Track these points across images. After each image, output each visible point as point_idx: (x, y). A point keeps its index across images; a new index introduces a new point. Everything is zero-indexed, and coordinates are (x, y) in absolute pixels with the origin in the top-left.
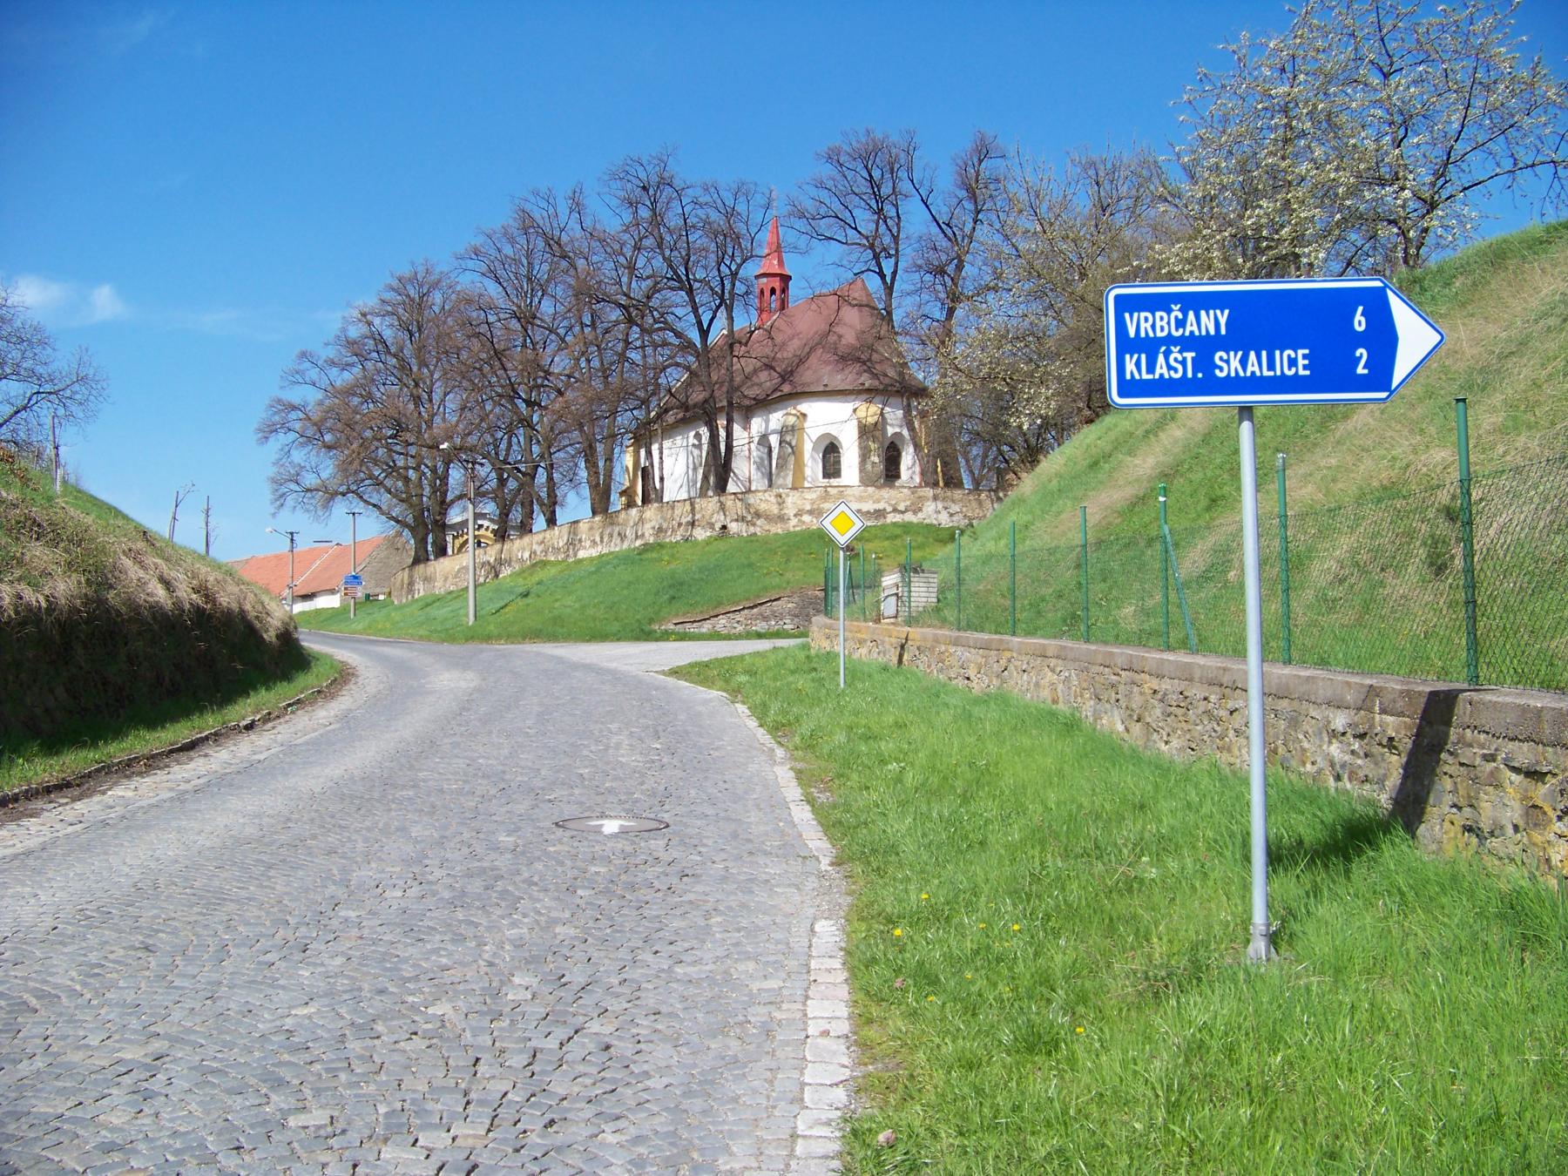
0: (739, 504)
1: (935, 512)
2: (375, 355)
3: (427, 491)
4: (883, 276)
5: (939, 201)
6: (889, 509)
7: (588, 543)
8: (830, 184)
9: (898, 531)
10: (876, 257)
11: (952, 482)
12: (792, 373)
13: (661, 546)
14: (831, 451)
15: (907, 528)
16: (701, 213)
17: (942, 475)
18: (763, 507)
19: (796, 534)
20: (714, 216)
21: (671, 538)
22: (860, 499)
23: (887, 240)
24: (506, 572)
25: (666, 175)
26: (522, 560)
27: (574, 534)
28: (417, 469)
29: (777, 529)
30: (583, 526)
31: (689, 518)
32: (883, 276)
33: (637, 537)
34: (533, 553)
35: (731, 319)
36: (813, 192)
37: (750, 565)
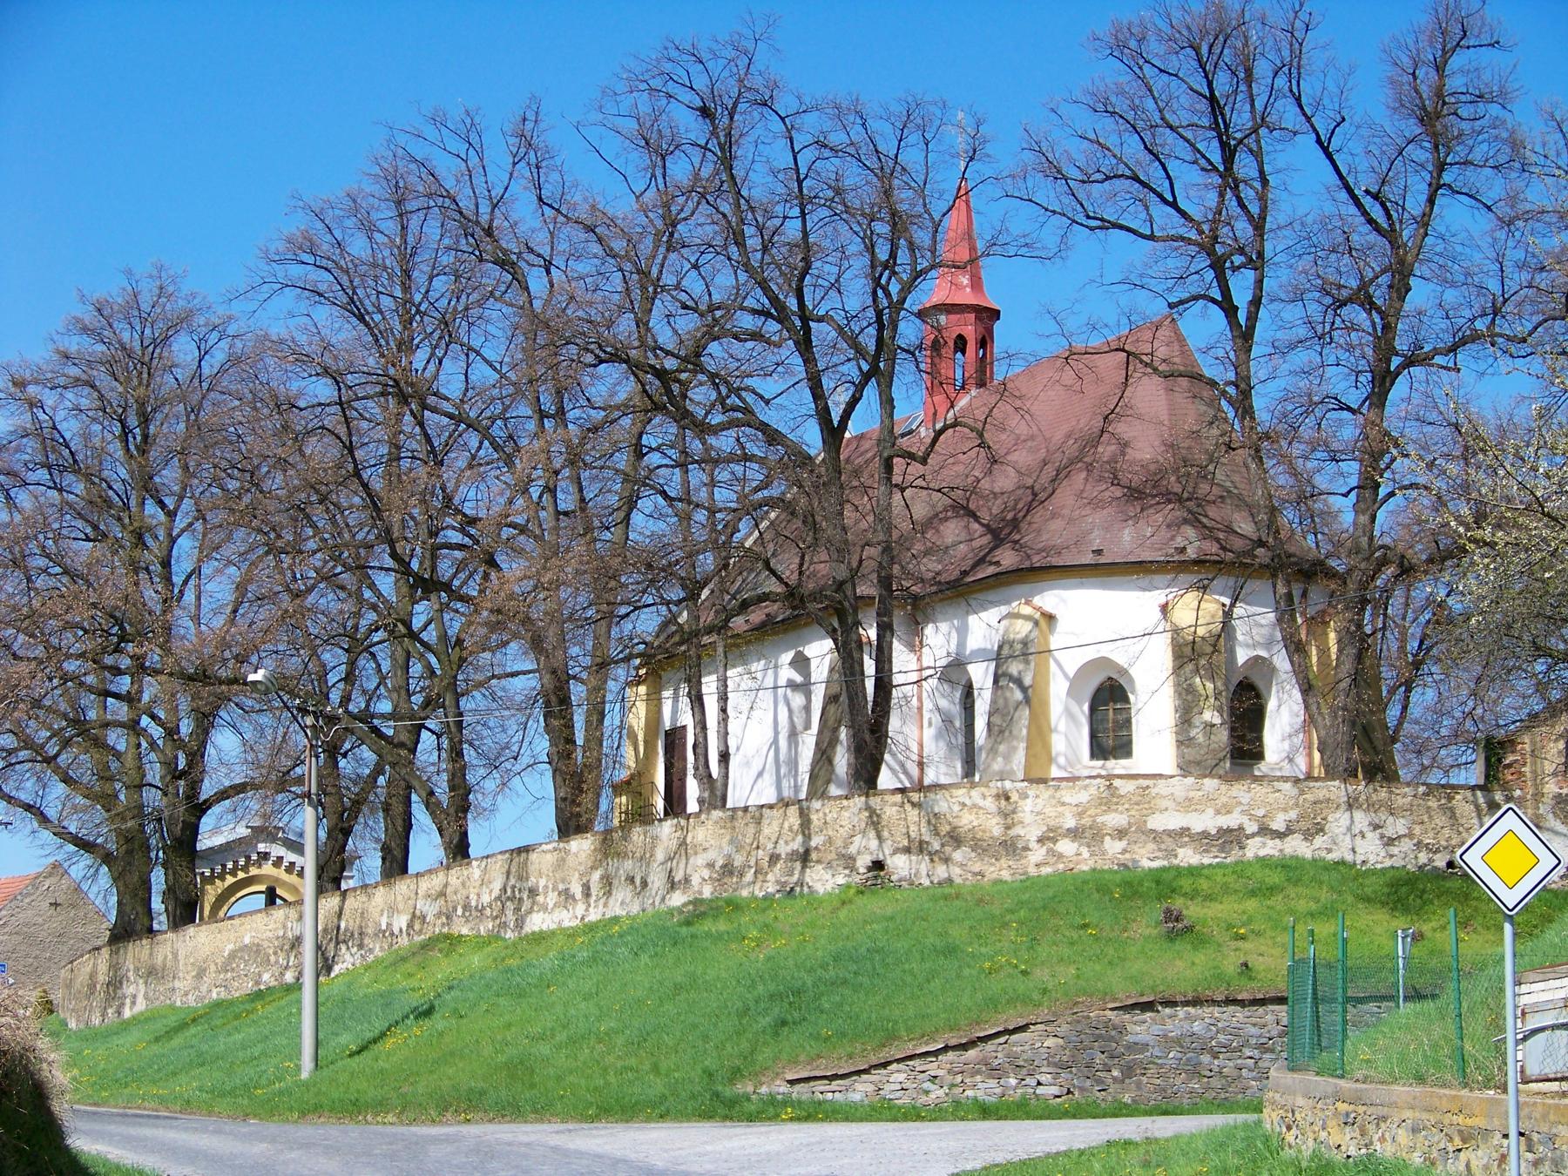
0: (913, 814)
1: (1359, 836)
2: (42, 474)
3: (155, 773)
4: (1230, 310)
5: (1356, 147)
6: (1251, 828)
7: (552, 898)
8: (1121, 105)
9: (1275, 878)
10: (1218, 266)
11: (1378, 770)
12: (1015, 524)
13: (735, 906)
14: (1109, 698)
15: (1291, 869)
16: (829, 167)
17: (1365, 750)
18: (967, 820)
19: (1046, 882)
20: (853, 176)
21: (749, 889)
22: (1188, 805)
23: (1243, 229)
24: (347, 960)
25: (756, 81)
26: (388, 934)
27: (519, 870)
28: (133, 726)
29: (1000, 870)
30: (542, 861)
31: (797, 844)
32: (1230, 310)
33: (672, 885)
34: (417, 918)
35: (888, 403)
36: (1086, 121)
37: (950, 951)
